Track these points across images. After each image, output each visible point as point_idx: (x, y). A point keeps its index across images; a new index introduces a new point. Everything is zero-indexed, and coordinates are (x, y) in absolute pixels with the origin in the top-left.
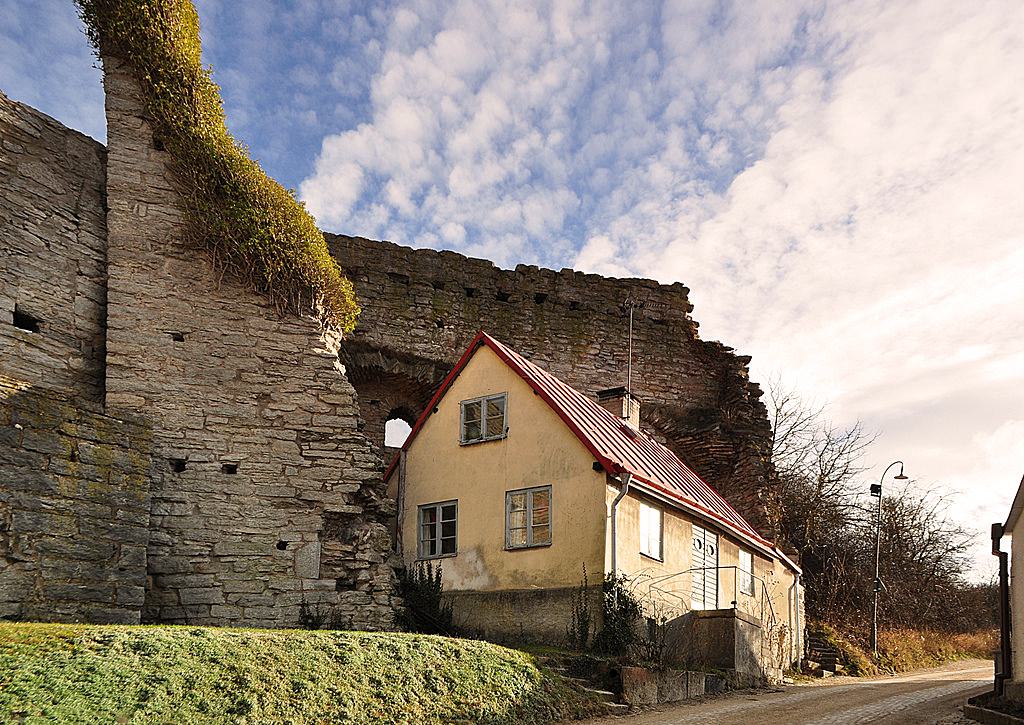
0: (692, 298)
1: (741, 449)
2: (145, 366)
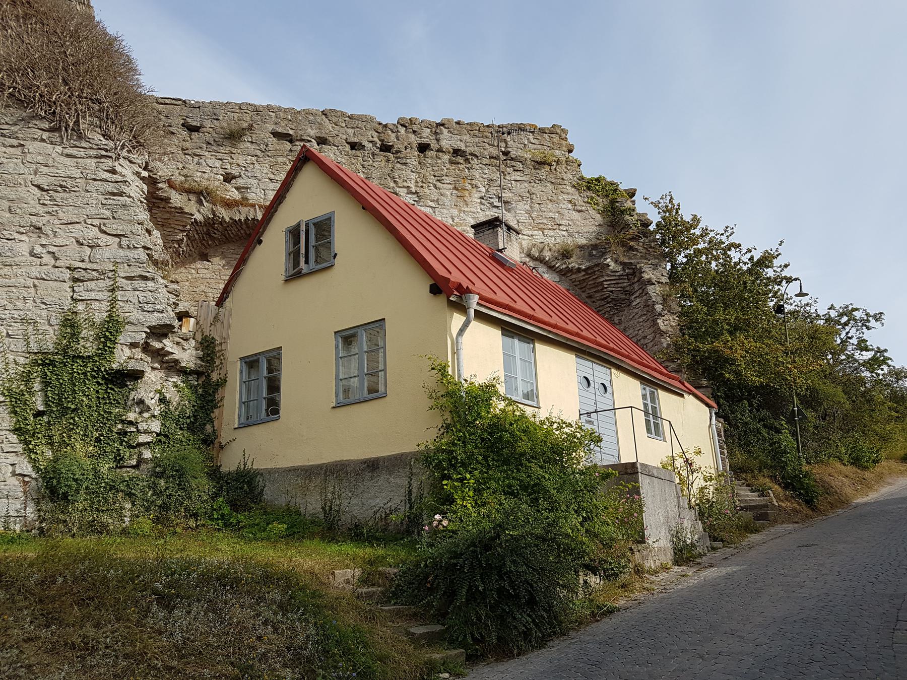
1: (636, 279)
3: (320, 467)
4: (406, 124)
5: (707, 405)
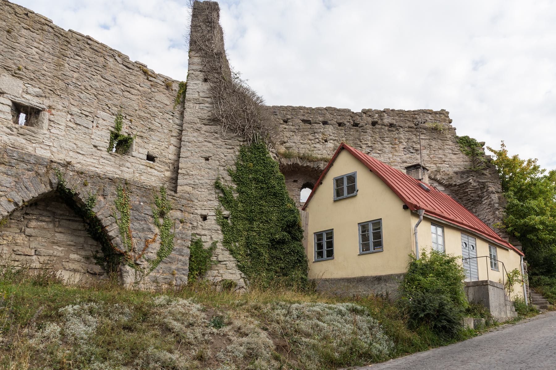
0: (451, 116)
1: (485, 190)
2: (193, 173)
3: (354, 279)
4: (365, 112)
5: (520, 254)
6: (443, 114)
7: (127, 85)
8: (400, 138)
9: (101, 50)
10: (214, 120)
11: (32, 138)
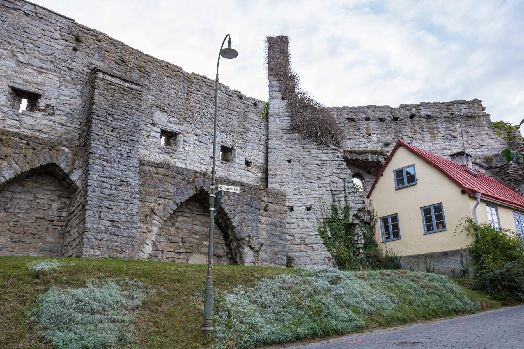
0: (484, 104)
3: (422, 255)
4: (403, 107)
6: (477, 102)
7: (230, 109)
8: (438, 128)
9: (212, 85)
10: (292, 129)
11: (173, 155)
